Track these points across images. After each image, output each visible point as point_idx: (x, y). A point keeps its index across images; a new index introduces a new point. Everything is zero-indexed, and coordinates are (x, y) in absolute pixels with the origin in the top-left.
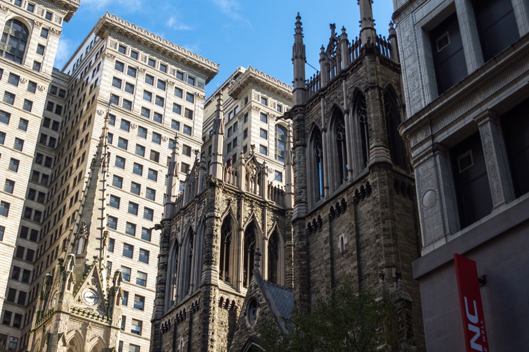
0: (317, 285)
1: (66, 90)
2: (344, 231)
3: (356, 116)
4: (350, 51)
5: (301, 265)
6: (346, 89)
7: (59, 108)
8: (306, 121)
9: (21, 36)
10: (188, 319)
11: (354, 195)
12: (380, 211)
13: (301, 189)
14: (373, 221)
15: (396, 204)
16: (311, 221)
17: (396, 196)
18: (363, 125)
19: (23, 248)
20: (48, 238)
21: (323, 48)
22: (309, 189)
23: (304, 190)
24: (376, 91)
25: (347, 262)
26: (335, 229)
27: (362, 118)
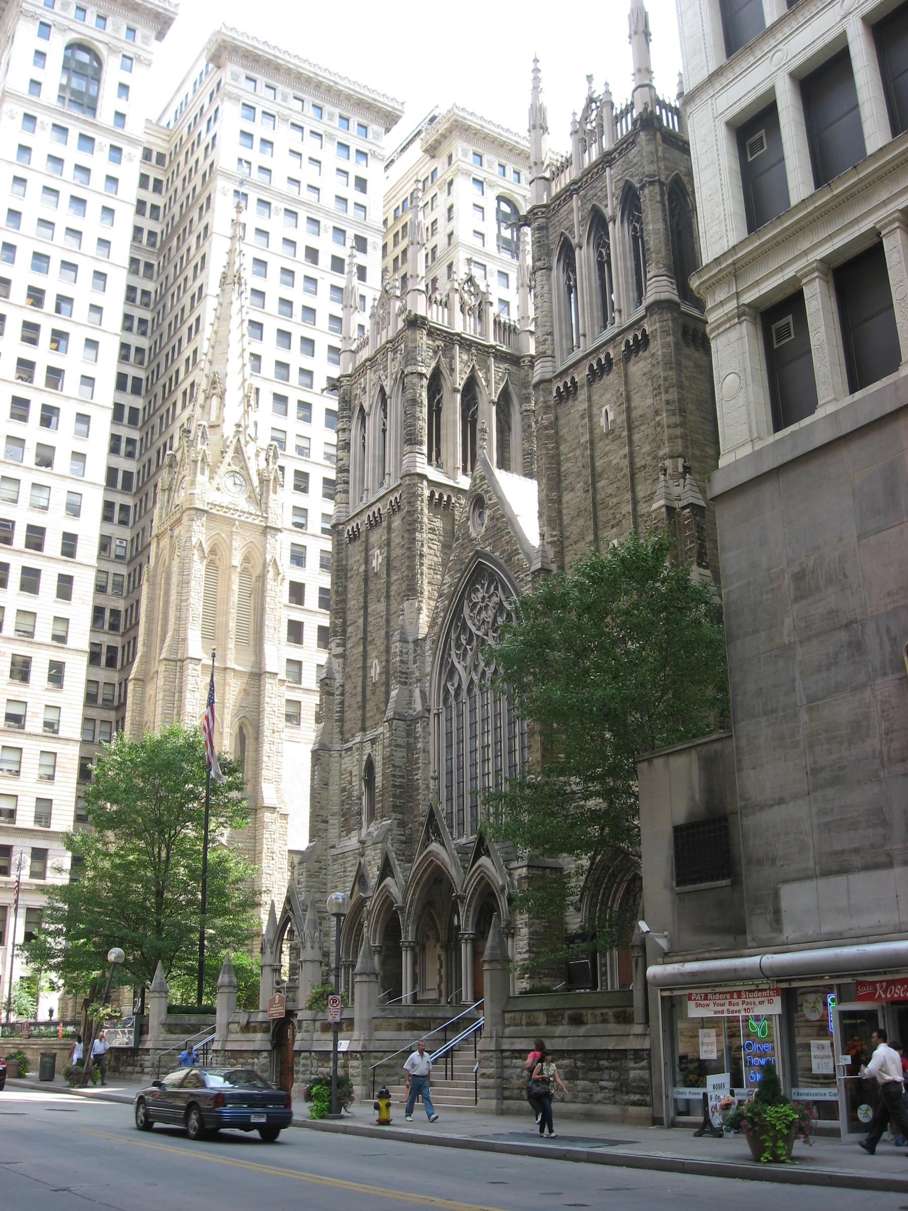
0: (571, 479)
1: (167, 153)
2: (608, 402)
3: (626, 225)
4: (617, 119)
5: (548, 449)
6: (611, 182)
7: (158, 182)
8: (551, 230)
9: (90, 72)
10: (384, 524)
12: (662, 374)
13: (545, 320)
14: (651, 388)
15: (685, 362)
16: (561, 385)
17: (686, 350)
18: (637, 239)
21: (575, 114)
22: (557, 336)
24: (657, 188)
25: (613, 447)
26: (595, 398)
27: (635, 229)
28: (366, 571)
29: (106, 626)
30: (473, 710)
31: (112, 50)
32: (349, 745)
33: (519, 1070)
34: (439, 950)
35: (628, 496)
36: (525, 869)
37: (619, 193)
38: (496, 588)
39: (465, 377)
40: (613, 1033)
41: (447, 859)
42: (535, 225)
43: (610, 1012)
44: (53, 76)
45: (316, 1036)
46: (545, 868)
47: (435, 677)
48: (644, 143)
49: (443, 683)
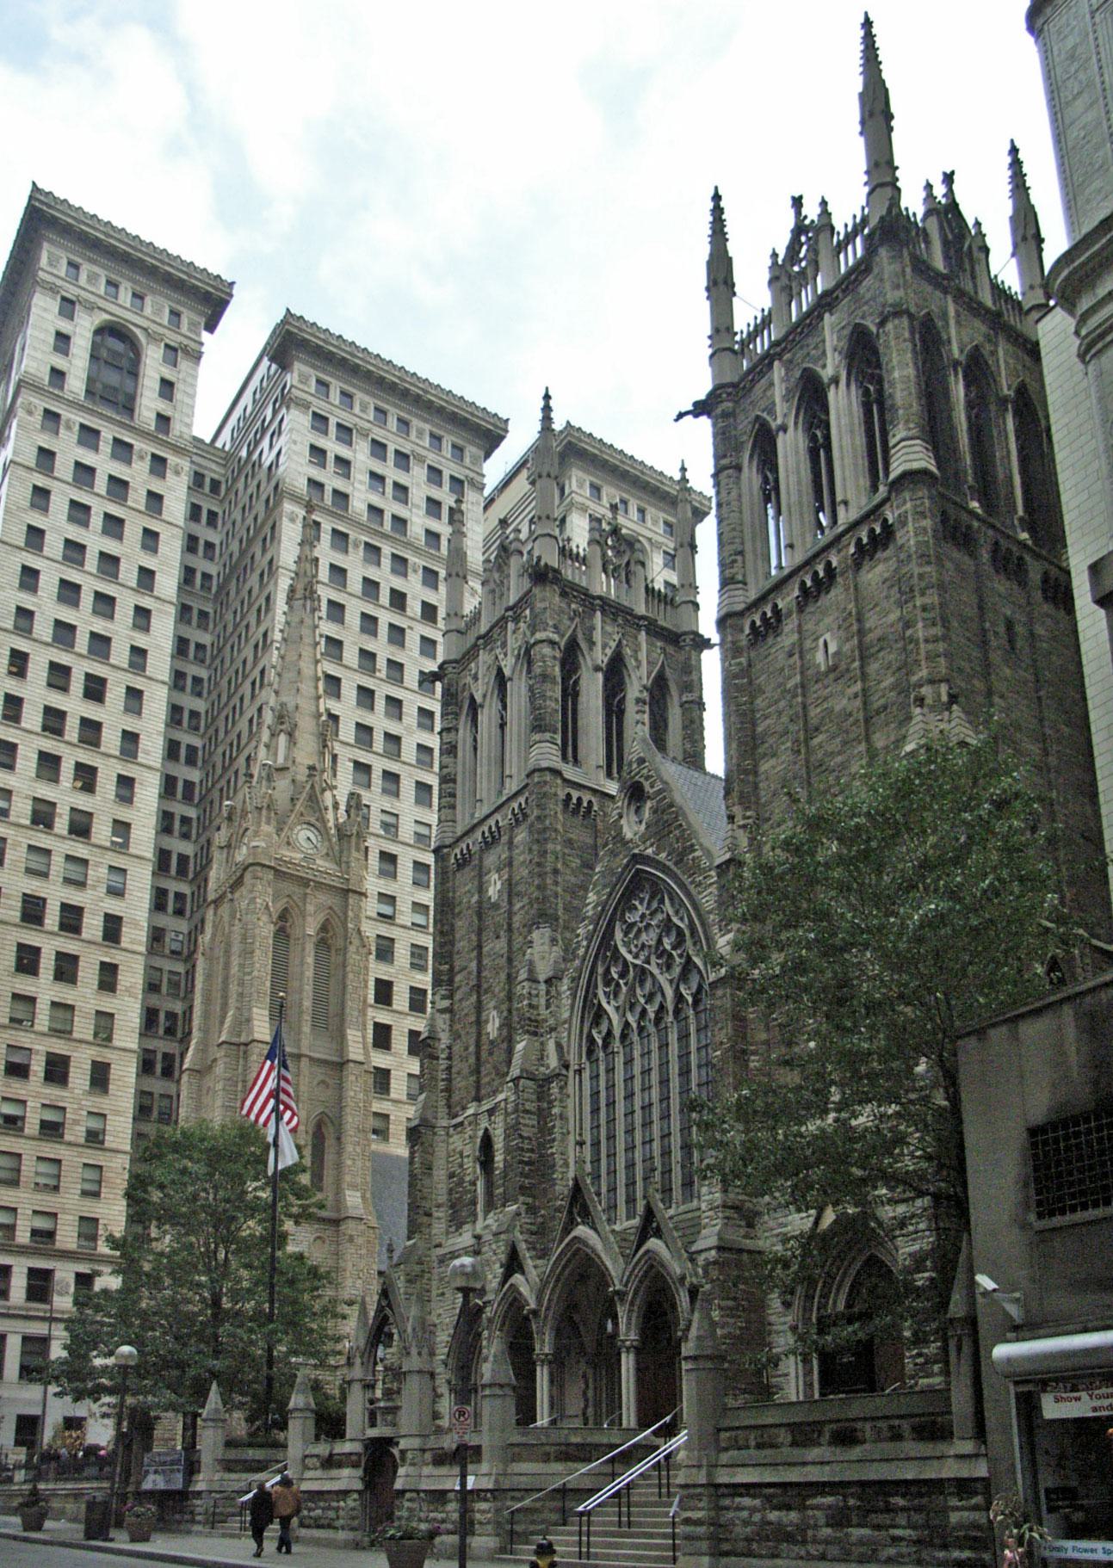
3: (853, 387)
4: (841, 247)
7: (212, 515)
8: (741, 417)
9: (124, 363)
10: (504, 839)
11: (852, 550)
19: (175, 779)
20: (221, 723)
21: (775, 255)
23: (739, 558)
24: (905, 321)
26: (809, 626)
28: (480, 902)
29: (161, 1031)
30: (629, 1062)
31: (153, 337)
32: (459, 1119)
33: (745, 1514)
34: (583, 1366)
35: (862, 747)
36: (713, 1252)
37: (844, 344)
38: (662, 901)
39: (609, 652)
40: (912, 1454)
41: (599, 1246)
42: (719, 411)
43: (906, 1426)
44: (78, 367)
45: (427, 1470)
46: (740, 1251)
47: (576, 1022)
48: (885, 260)
49: (585, 1031)
